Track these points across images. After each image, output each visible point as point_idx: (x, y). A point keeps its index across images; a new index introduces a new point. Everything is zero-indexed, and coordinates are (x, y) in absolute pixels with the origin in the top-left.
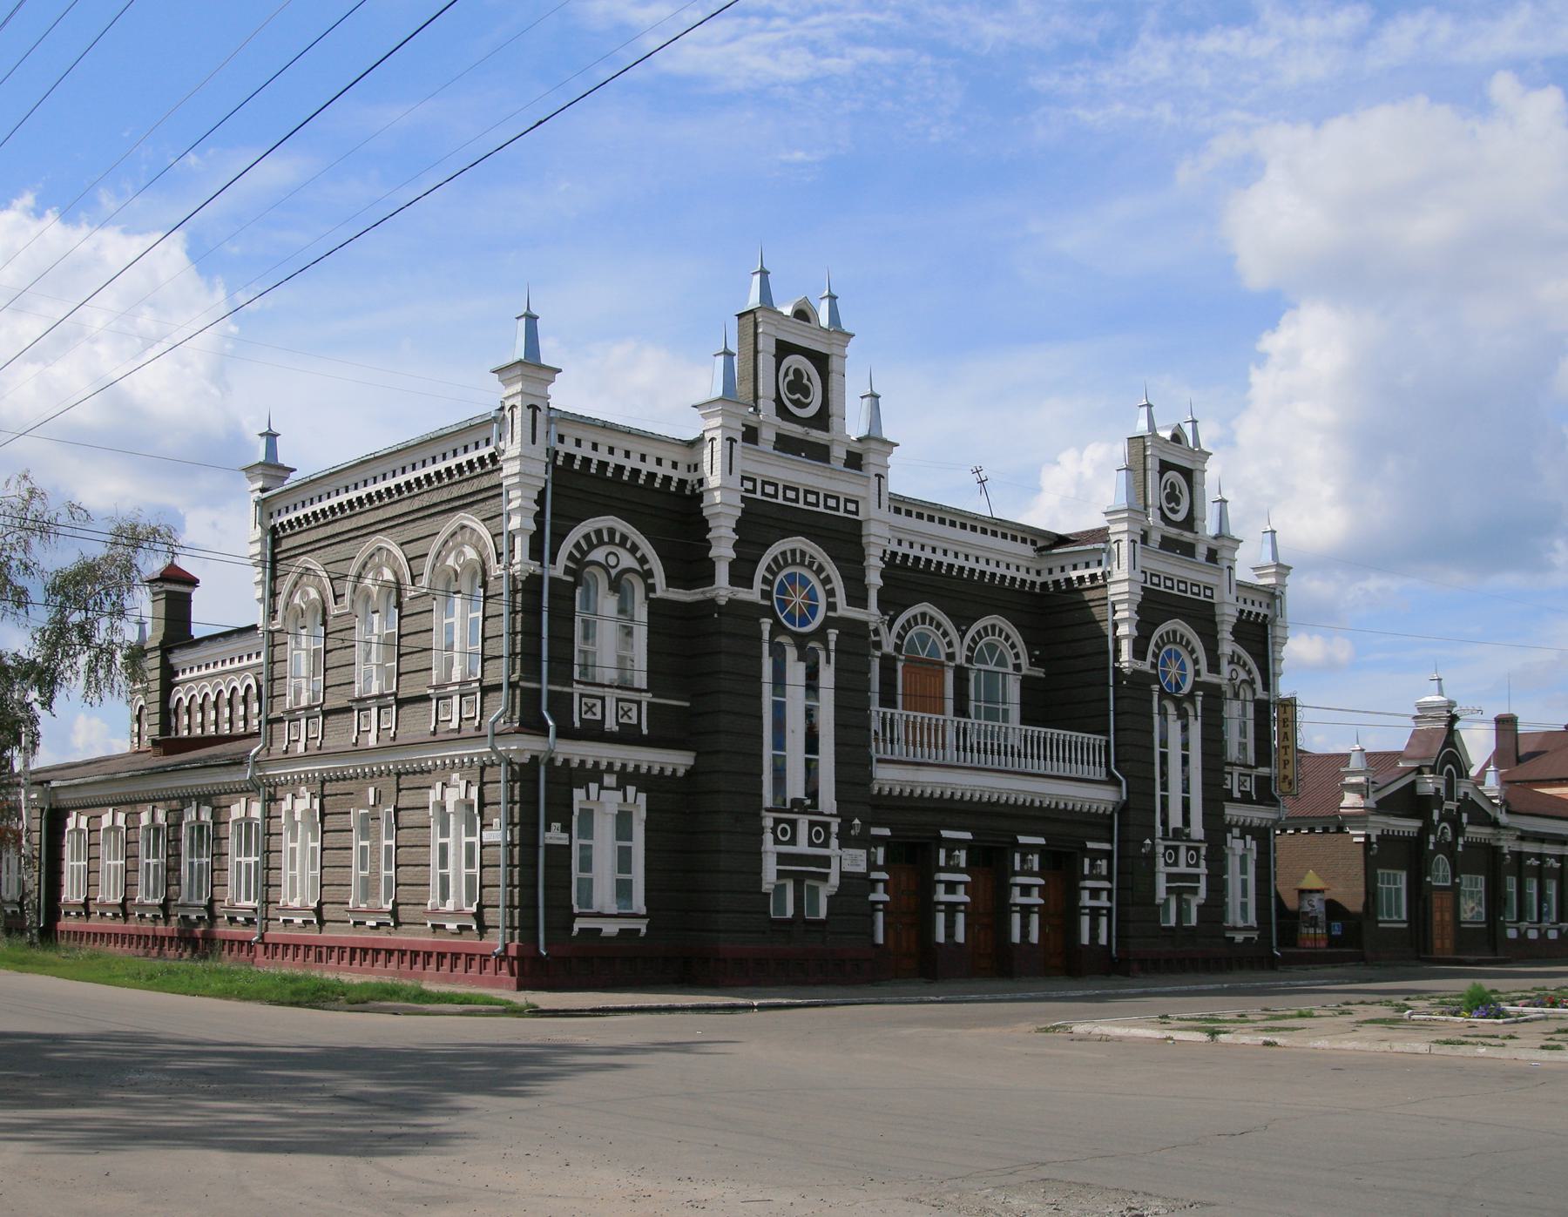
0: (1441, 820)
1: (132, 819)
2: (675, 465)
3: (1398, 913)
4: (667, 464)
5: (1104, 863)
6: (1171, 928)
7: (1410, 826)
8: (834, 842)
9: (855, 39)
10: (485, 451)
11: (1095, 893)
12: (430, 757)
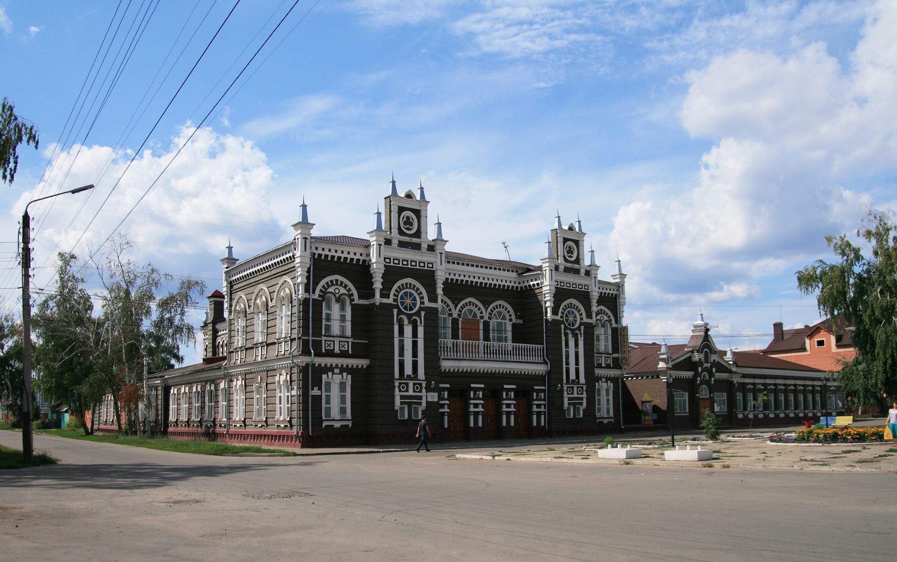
0: (703, 371)
1: (191, 388)
2: (361, 255)
3: (685, 409)
4: (358, 254)
7: (689, 374)
8: (424, 391)
9: (568, 31)
10: (291, 254)
11: (539, 406)
12: (276, 365)
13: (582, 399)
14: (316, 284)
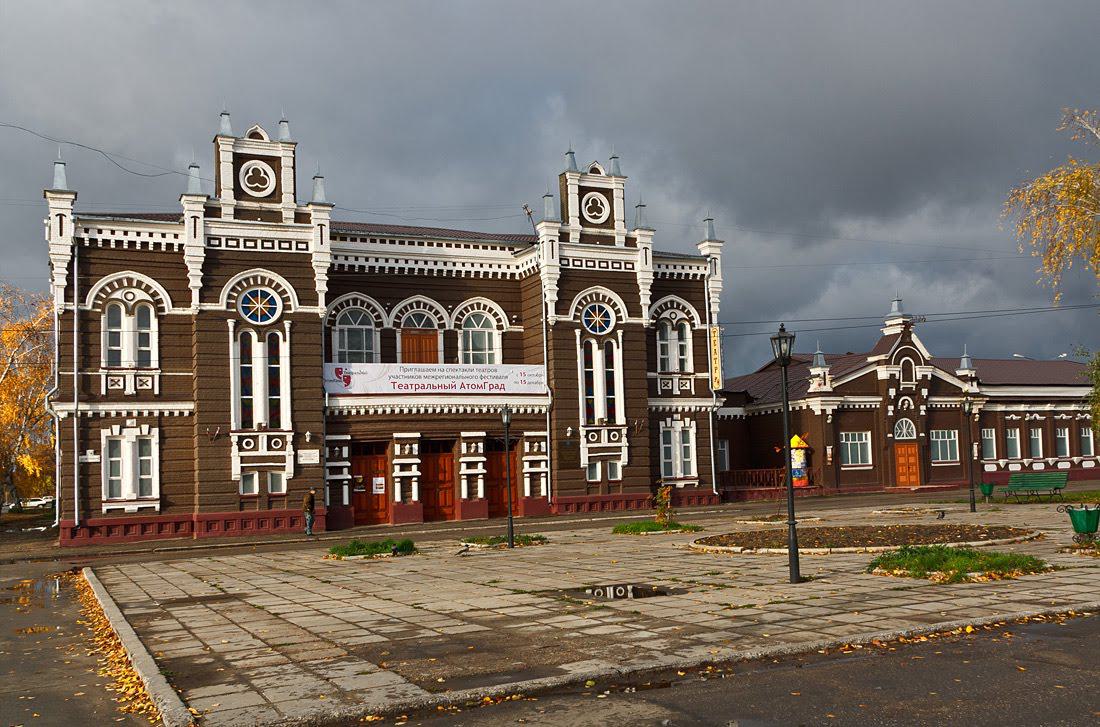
3: (864, 459)
6: (254, 497)
13: (619, 449)
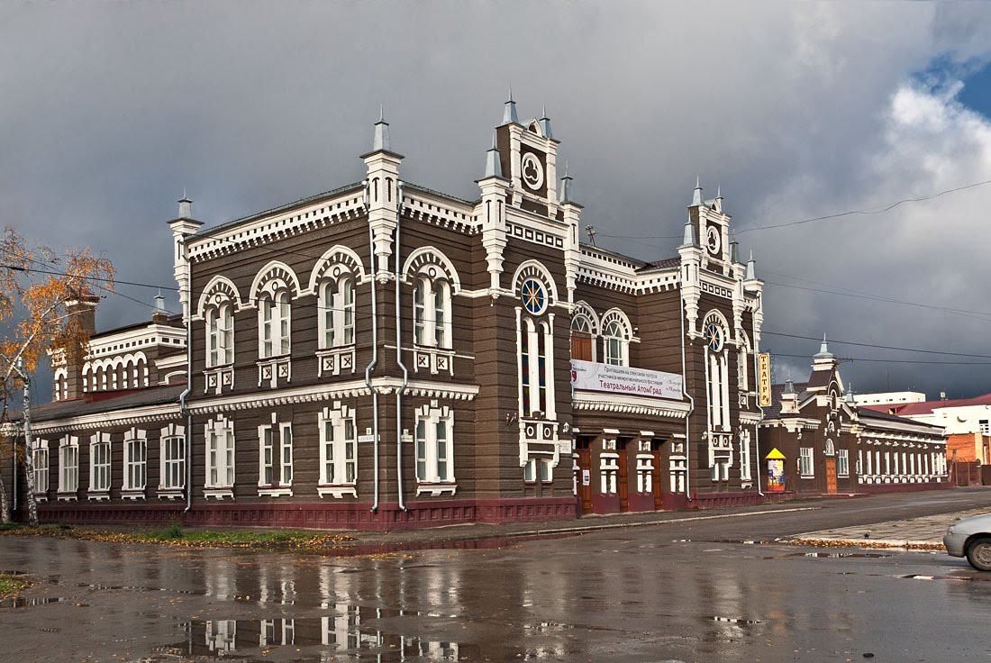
5: (681, 445)
8: (555, 436)
11: (677, 462)
14: (403, 259)
